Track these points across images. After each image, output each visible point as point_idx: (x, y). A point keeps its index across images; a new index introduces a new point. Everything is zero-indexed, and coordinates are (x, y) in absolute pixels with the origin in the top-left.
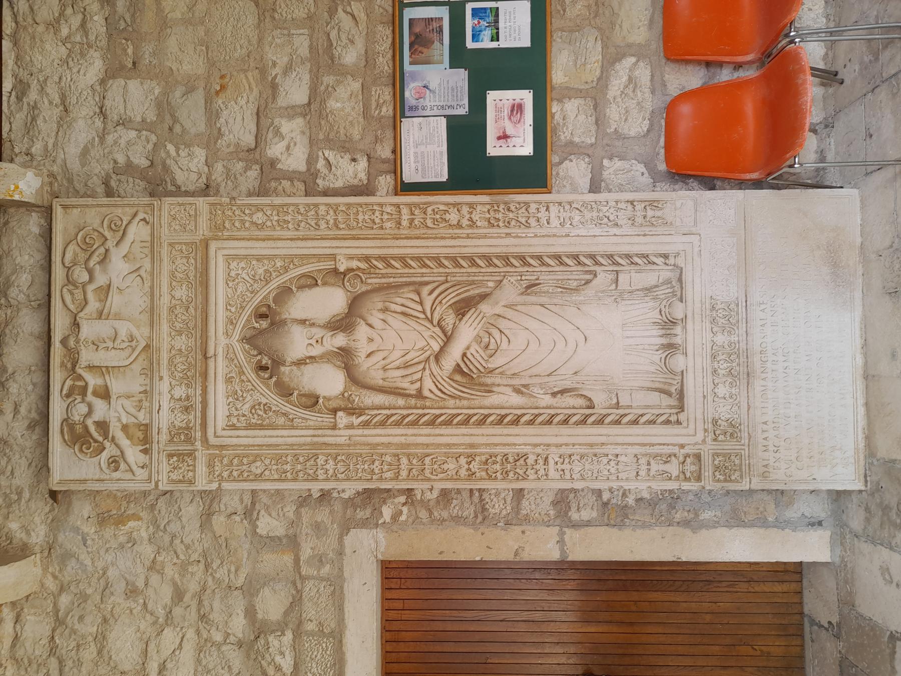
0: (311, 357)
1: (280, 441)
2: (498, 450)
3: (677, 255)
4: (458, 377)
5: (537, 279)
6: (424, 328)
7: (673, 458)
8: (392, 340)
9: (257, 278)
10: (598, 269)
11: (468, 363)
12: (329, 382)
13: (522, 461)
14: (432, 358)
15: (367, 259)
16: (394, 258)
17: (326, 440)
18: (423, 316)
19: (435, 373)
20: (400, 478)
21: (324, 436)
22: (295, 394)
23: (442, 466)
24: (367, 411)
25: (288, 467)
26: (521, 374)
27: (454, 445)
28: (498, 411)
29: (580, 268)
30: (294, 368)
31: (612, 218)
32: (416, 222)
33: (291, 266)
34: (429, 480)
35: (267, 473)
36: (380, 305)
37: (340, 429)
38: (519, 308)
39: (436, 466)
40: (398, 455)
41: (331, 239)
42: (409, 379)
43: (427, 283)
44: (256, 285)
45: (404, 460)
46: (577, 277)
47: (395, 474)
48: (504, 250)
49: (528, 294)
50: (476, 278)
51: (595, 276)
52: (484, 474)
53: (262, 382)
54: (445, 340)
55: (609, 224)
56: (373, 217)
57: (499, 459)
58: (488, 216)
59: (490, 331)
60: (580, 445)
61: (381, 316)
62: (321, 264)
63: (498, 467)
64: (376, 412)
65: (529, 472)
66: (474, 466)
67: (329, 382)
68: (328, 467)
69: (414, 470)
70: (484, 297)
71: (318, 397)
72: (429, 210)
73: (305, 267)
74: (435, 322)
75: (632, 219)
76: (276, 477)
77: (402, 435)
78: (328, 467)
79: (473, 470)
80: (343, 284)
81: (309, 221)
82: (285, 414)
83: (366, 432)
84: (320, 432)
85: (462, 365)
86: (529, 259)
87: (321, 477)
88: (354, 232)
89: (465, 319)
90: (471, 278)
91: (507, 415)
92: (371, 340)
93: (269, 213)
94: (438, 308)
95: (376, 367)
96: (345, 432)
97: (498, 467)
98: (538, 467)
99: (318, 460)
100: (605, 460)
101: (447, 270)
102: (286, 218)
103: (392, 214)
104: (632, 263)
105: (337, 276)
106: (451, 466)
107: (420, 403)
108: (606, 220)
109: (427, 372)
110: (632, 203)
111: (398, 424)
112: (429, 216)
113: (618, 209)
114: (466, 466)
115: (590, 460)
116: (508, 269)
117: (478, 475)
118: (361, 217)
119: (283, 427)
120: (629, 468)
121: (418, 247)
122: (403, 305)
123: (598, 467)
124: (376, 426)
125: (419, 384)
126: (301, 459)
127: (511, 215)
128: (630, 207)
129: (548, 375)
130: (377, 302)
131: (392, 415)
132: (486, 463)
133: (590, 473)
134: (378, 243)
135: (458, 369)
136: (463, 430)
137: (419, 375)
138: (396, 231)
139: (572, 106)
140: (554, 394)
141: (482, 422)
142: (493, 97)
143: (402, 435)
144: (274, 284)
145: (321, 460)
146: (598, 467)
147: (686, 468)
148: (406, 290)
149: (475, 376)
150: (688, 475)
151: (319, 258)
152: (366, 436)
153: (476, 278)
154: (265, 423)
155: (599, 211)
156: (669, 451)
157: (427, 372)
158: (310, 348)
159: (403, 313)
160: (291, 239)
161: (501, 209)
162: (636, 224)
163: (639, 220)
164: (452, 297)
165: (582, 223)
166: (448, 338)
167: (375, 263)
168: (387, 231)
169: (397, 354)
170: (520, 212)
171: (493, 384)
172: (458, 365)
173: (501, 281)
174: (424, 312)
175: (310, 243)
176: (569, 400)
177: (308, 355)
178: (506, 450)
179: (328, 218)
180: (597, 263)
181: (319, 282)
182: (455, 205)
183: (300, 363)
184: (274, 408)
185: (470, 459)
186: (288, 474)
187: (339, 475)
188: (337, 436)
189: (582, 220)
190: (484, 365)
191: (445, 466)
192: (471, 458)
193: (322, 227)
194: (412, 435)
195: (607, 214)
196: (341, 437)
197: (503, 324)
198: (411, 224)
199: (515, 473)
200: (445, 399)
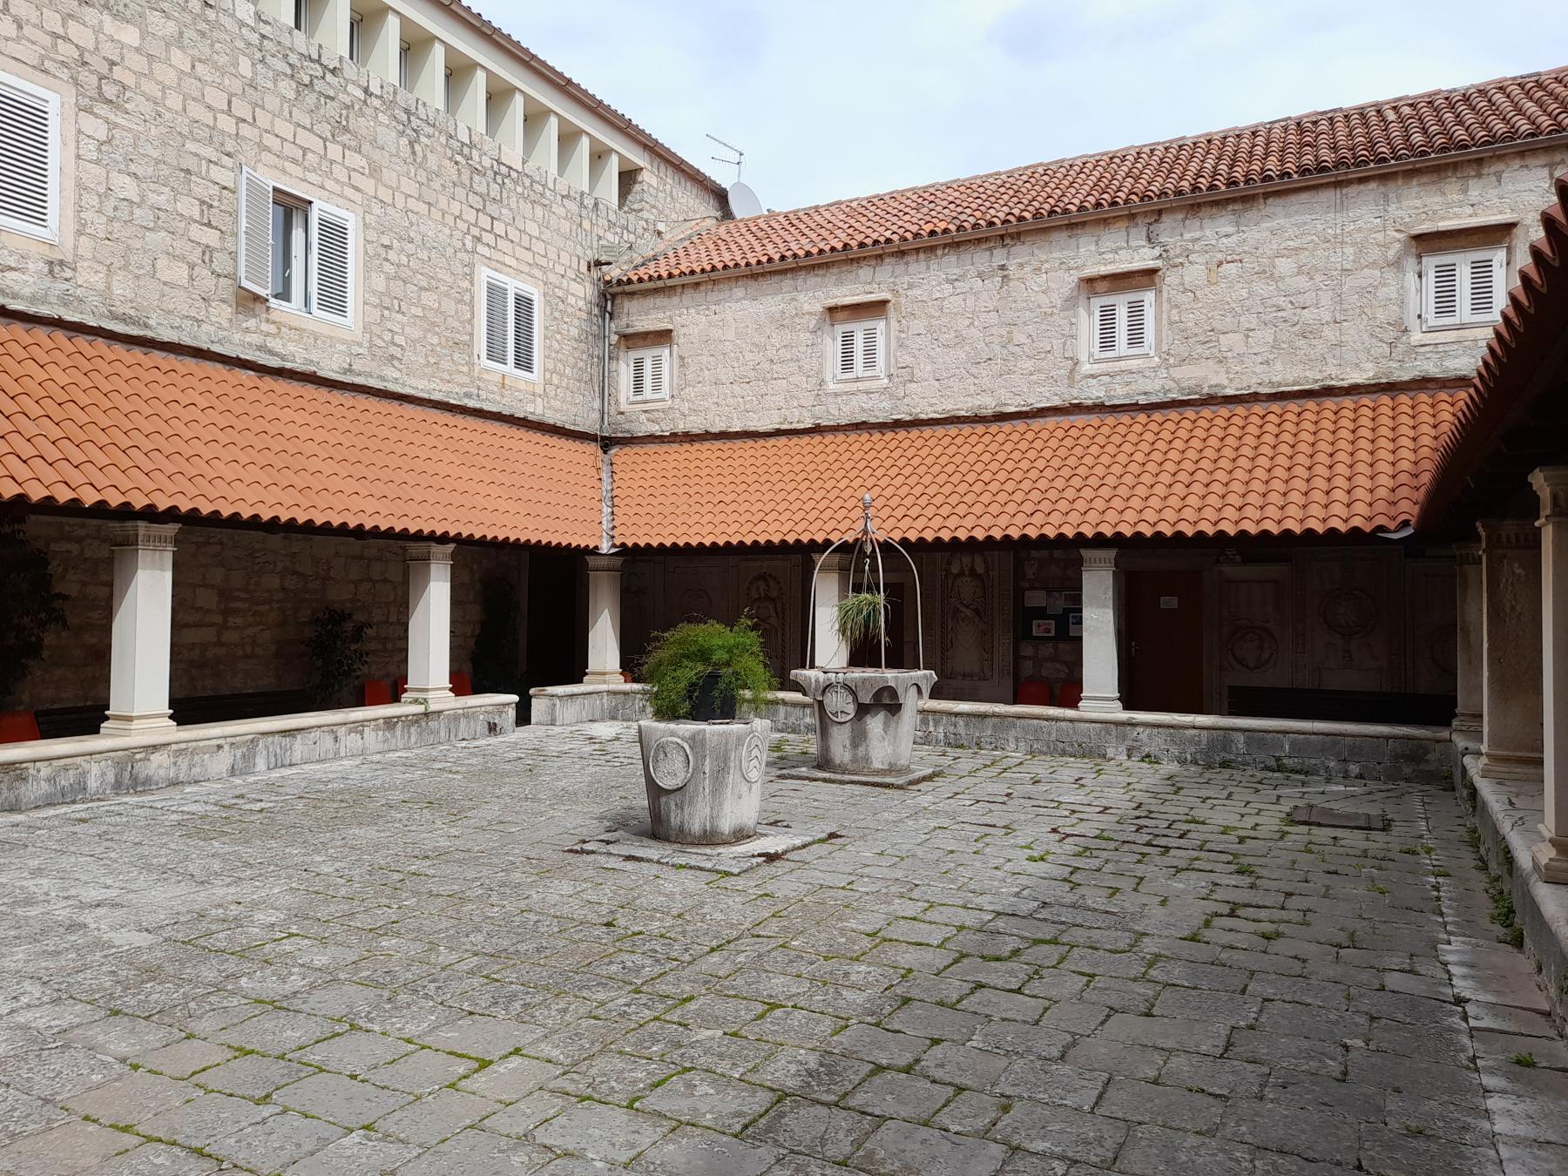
12: (955, 569)
67: (955, 569)
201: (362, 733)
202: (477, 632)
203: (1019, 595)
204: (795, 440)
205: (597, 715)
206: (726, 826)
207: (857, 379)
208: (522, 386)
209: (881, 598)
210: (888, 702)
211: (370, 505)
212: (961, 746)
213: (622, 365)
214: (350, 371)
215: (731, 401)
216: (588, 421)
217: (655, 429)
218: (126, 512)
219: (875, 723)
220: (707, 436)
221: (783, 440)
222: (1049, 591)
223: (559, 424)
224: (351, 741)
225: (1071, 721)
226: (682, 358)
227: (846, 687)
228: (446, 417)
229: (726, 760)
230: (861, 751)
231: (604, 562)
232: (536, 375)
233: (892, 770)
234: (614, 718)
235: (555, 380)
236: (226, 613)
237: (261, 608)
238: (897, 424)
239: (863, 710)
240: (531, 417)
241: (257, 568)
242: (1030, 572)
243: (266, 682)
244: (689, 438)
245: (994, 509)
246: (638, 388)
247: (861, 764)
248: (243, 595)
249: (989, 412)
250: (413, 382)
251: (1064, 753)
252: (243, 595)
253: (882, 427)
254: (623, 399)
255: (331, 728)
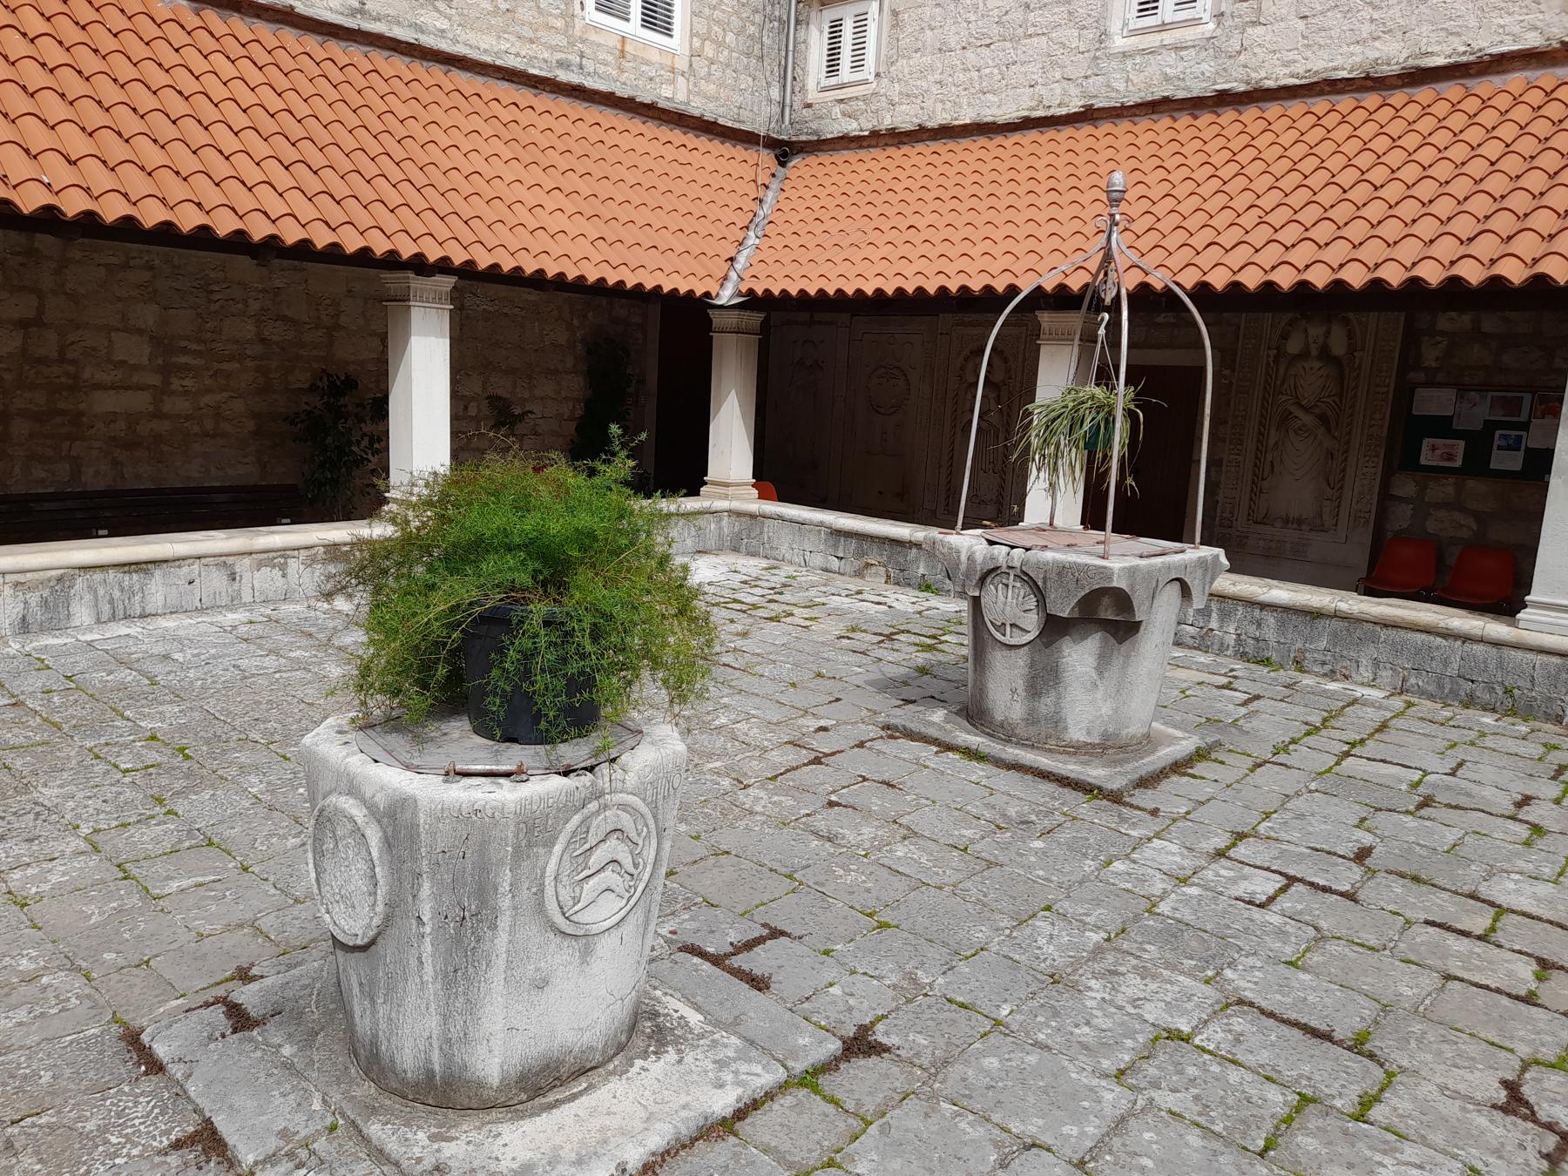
8: (1312, 381)
12: (1293, 346)
15: (1359, 368)
67: (1293, 346)
70: (1329, 430)
139: (1450, 490)
142: (1461, 444)
166: (1307, 410)
176: (1267, 470)
201: (283, 568)
202: (579, 413)
203: (1405, 393)
204: (1051, 133)
205: (712, 544)
206: (491, 1062)
207: (1163, 27)
208: (655, 57)
209: (1122, 395)
210: (1109, 615)
211: (580, 248)
212: (1266, 662)
213: (813, 29)
214: (362, 12)
215: (961, 77)
216: (759, 120)
217: (852, 127)
218: (392, 261)
219: (1079, 656)
220: (921, 134)
221: (1033, 134)
222: (1462, 389)
223: (709, 116)
224: (267, 580)
225: (1497, 644)
226: (895, 13)
227: (1025, 577)
228: (525, 96)
229: (484, 891)
230: (1046, 704)
231: (732, 319)
232: (678, 42)
233: (1108, 747)
234: (736, 550)
235: (709, 50)
236: (167, 371)
237: (225, 366)
238: (1224, 99)
239: (1054, 628)
240: (662, 104)
241: (213, 307)
242: (1431, 355)
243: (241, 470)
244: (896, 138)
245: (1391, 230)
246: (833, 66)
247: (1045, 730)
248: (194, 346)
249: (1394, 69)
250: (472, 37)
251: (1469, 702)
252: (194, 346)
253: (1195, 105)
254: (811, 84)
255: (223, 561)
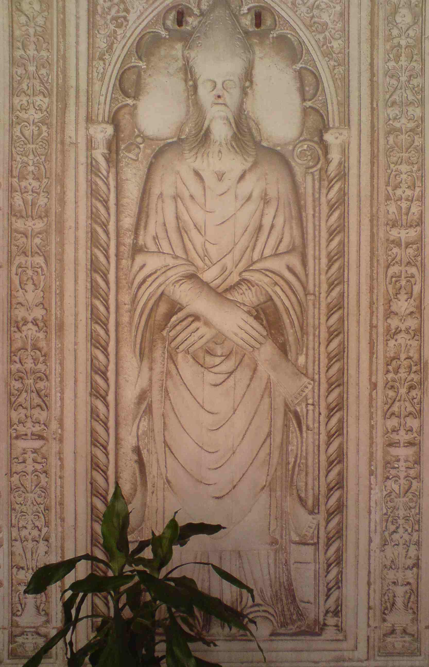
0: (195, 87)
1: (71, 39)
2: (54, 363)
3: (339, 628)
4: (163, 309)
5: (308, 428)
6: (237, 258)
7: (44, 619)
9: (315, 12)
10: (322, 517)
11: (184, 323)
12: (158, 113)
13: (37, 400)
14: (191, 269)
15: (343, 175)
16: (343, 217)
17: (72, 108)
18: (256, 256)
19: (169, 273)
20: (14, 219)
21: (77, 104)
22: (141, 64)
23: (30, 283)
24: (113, 170)
25: (31, 52)
26: (168, 402)
27: (62, 300)
28: (112, 367)
29: (323, 489)
30: (180, 63)
31: (396, 537)
32: (395, 250)
33: (332, 63)
34: (10, 262)
35: (23, 19)
36: (272, 193)
37: (87, 129)
38: (266, 400)
39: (30, 272)
40: (47, 216)
41: (372, 122)
42: (161, 235)
43: (304, 264)
44: (304, 9)
45: (39, 225)
46: (310, 486)
47: (20, 211)
48: (352, 381)
49: (286, 414)
50: (311, 338)
51: (311, 512)
52: (19, 344)
53: (158, 14)
54: (220, 290)
55: (386, 533)
56: (404, 186)
57: (41, 367)
58: (403, 356)
59: (233, 358)
60: (62, 487)
61: (256, 194)
62: (336, 107)
63: (29, 364)
64: (112, 183)
65: (23, 412)
66: (30, 331)
68: (32, 111)
69: (24, 240)
70: (283, 349)
71: (136, 97)
72: (413, 270)
73: (331, 83)
74: (246, 275)
75: (393, 566)
76: (17, 33)
77: (77, 223)
78: (32, 111)
79: (24, 328)
80: (305, 140)
81: (398, 92)
82: (110, 47)
83: (82, 169)
84: (83, 99)
85: (180, 315)
86: (338, 415)
87: (16, 100)
88: (382, 158)
89: (251, 320)
90: (311, 330)
91: (106, 380)
92: (220, 177)
93: (411, 33)
94: (266, 280)
95: (180, 185)
96: (86, 136)
97: (29, 364)
98: (29, 424)
99: (41, 97)
100: (40, 523)
101: (323, 295)
102: (403, 58)
103: (407, 214)
104: (329, 565)
105: (316, 125)
106: (31, 296)
107: (126, 250)
108: (392, 528)
109: (171, 262)
110: (417, 565)
111: (93, 216)
112: (403, 268)
113: (407, 545)
114: (30, 319)
115: (39, 500)
116: (324, 386)
117: (18, 335)
118: (404, 168)
119: (91, 45)
120: (29, 556)
121: (359, 251)
122: (272, 227)
123: (30, 512)
124: (91, 184)
125: (153, 248)
126: (43, 71)
127: (403, 391)
128: (410, 562)
129: (165, 442)
130: (277, 185)
131: (107, 209)
132: (35, 347)
133: (20, 500)
134: (366, 192)
135: (175, 308)
136: (84, 315)
137: (166, 248)
138: (382, 220)
140: (137, 451)
141: (96, 342)
143: (77, 223)
144: (305, 35)
145: (39, 100)
146: (30, 512)
147: (30, 636)
148: (296, 233)
149: (164, 333)
150: (20, 640)
151: (345, 103)
152: (76, 168)
153: (311, 338)
154: (98, 18)
155: (406, 519)
156: (53, 613)
157: (171, 262)
158: (209, 86)
159: (260, 228)
160: (372, 65)
161: (412, 375)
162: (385, 571)
163: (391, 575)
164: (282, 299)
165: (389, 494)
166: (222, 294)
167: (336, 188)
168: (382, 208)
169: (199, 215)
170: (407, 404)
171: (152, 361)
172: (180, 309)
173: (306, 375)
174: (262, 258)
175: (365, 91)
177: (200, 82)
178: (54, 379)
179: (403, 120)
180: (330, 515)
181: (309, 104)
182: (420, 307)
183: (188, 72)
184: (119, 31)
185: (41, 324)
186: (21, 52)
187: (19, 127)
188: (77, 123)
189: (393, 495)
190: (181, 348)
191: (30, 287)
192: (42, 325)
193: (389, 110)
194: (76, 238)
195: (401, 530)
196: (75, 131)
197: (243, 376)
198: (393, 242)
199: (20, 391)
200: (130, 288)
